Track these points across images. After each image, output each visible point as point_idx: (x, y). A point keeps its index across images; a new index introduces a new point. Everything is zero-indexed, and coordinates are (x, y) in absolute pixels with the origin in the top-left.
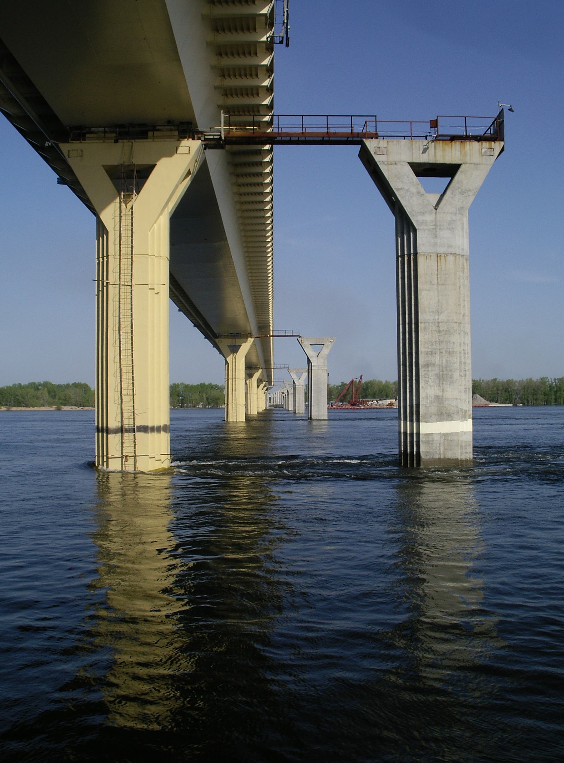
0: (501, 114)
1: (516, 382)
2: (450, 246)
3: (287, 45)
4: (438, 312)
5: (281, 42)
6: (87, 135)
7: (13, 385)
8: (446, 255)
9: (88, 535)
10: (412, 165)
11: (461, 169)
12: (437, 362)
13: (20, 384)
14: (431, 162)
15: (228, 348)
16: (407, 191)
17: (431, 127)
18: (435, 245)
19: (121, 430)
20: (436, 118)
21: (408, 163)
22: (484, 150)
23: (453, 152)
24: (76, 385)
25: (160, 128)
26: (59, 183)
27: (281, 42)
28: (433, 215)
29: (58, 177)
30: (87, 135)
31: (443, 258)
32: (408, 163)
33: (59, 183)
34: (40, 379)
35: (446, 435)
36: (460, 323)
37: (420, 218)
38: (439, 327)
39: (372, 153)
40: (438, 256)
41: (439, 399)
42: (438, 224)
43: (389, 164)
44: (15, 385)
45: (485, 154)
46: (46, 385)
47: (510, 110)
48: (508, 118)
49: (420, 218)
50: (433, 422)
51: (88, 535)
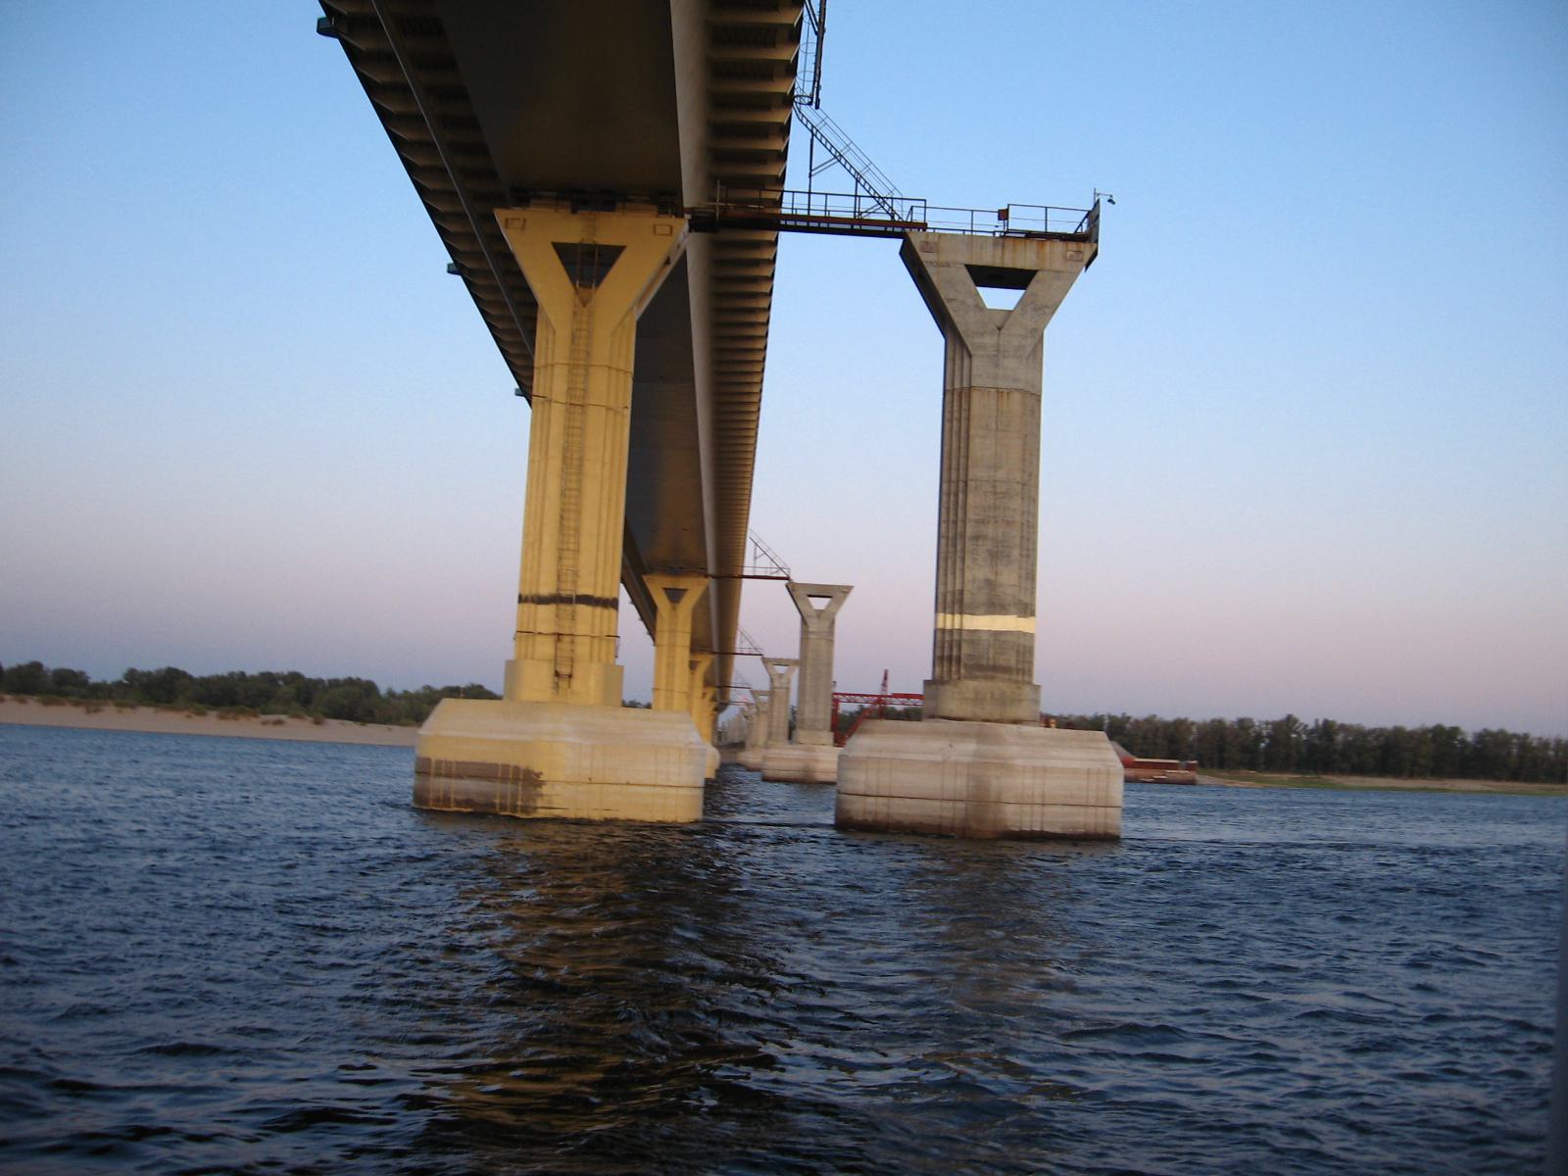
0: (1097, 204)
1: (1193, 723)
2: (1015, 380)
3: (817, 107)
4: (996, 467)
5: (810, 104)
6: (533, 201)
8: (1010, 391)
10: (969, 267)
11: (1037, 277)
12: (990, 535)
13: (243, 674)
15: (663, 592)
16: (963, 303)
17: (1000, 219)
18: (995, 377)
19: (809, 210)
20: (1005, 207)
21: (967, 266)
22: (1069, 254)
25: (632, 197)
27: (810, 104)
28: (996, 337)
29: (451, 261)
30: (533, 201)
31: (1005, 395)
32: (967, 266)
34: (281, 666)
35: (997, 634)
36: (1024, 485)
37: (977, 340)
38: (994, 487)
39: (918, 249)
40: (999, 392)
41: (990, 584)
42: (1002, 349)
43: (939, 265)
44: (232, 675)
45: (1071, 259)
46: (295, 677)
47: (1110, 201)
48: (1106, 212)
49: (977, 340)
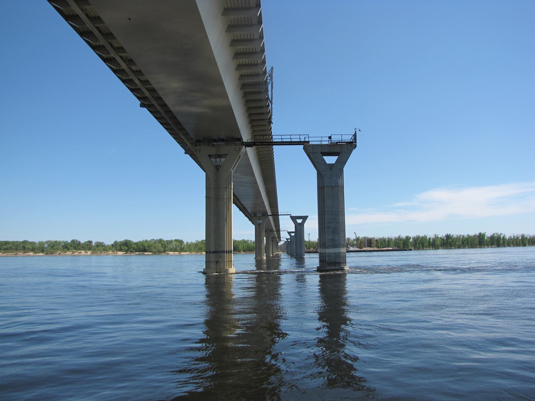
7: (143, 241)
9: (422, 291)
14: (329, 152)
23: (284, 278)
24: (176, 240)
26: (140, 107)
29: (141, 103)
33: (140, 107)
35: (335, 253)
38: (332, 213)
40: (332, 187)
44: (143, 241)
46: (160, 241)
47: (360, 131)
50: (331, 248)
51: (422, 291)
